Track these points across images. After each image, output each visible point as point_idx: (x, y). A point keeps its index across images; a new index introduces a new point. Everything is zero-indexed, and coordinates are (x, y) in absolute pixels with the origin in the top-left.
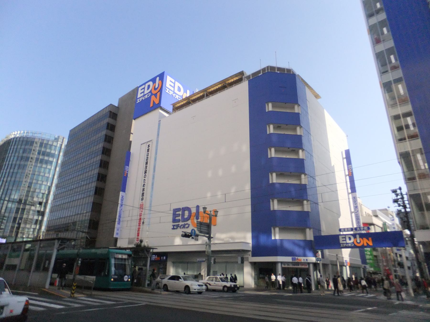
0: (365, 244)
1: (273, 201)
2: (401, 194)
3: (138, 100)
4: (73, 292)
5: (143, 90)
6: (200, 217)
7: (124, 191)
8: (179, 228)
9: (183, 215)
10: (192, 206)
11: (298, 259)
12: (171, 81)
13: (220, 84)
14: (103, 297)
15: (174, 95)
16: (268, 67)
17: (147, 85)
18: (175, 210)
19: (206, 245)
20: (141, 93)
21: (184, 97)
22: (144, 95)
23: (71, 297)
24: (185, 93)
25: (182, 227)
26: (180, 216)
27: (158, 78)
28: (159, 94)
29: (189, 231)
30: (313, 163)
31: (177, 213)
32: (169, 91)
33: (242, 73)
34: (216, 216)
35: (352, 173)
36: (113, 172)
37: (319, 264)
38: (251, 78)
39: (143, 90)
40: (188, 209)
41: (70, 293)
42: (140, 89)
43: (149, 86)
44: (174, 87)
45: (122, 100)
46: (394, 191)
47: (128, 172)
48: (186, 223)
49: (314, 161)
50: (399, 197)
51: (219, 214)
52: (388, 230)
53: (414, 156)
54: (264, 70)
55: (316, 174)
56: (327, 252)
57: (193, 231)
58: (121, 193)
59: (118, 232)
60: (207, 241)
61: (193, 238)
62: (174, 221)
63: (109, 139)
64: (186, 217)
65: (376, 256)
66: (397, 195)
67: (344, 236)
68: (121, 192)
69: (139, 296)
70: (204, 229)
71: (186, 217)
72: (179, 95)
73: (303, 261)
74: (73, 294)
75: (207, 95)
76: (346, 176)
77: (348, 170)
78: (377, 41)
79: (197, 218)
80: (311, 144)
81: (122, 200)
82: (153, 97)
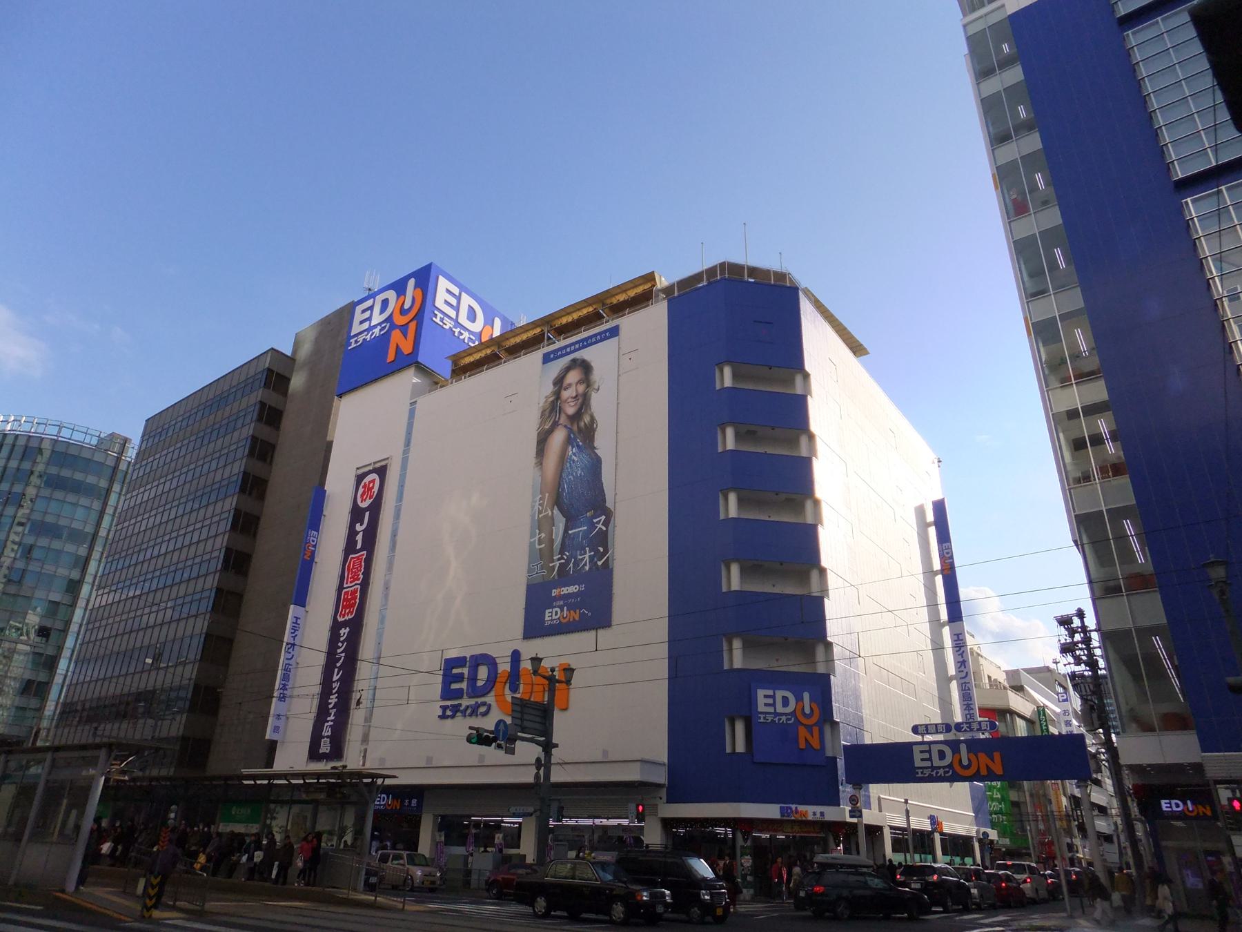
0: (984, 772)
2: (1084, 629)
3: (353, 341)
4: (149, 903)
9: (473, 678)
11: (797, 811)
12: (448, 291)
14: (234, 920)
15: (457, 331)
16: (722, 265)
18: (450, 664)
19: (538, 769)
20: (361, 322)
22: (371, 328)
24: (489, 327)
25: (469, 711)
26: (461, 680)
27: (412, 282)
28: (413, 326)
29: (488, 724)
32: (442, 320)
33: (650, 278)
34: (568, 682)
36: (269, 546)
39: (367, 314)
42: (359, 309)
43: (385, 303)
44: (457, 309)
46: (1064, 622)
47: (315, 546)
48: (480, 700)
50: (1078, 637)
52: (1054, 730)
54: (711, 271)
57: (502, 727)
59: (278, 723)
61: (499, 746)
62: (447, 693)
63: (262, 450)
64: (480, 683)
66: (1072, 632)
67: (926, 747)
68: (292, 606)
71: (480, 683)
73: (810, 817)
82: (396, 335)
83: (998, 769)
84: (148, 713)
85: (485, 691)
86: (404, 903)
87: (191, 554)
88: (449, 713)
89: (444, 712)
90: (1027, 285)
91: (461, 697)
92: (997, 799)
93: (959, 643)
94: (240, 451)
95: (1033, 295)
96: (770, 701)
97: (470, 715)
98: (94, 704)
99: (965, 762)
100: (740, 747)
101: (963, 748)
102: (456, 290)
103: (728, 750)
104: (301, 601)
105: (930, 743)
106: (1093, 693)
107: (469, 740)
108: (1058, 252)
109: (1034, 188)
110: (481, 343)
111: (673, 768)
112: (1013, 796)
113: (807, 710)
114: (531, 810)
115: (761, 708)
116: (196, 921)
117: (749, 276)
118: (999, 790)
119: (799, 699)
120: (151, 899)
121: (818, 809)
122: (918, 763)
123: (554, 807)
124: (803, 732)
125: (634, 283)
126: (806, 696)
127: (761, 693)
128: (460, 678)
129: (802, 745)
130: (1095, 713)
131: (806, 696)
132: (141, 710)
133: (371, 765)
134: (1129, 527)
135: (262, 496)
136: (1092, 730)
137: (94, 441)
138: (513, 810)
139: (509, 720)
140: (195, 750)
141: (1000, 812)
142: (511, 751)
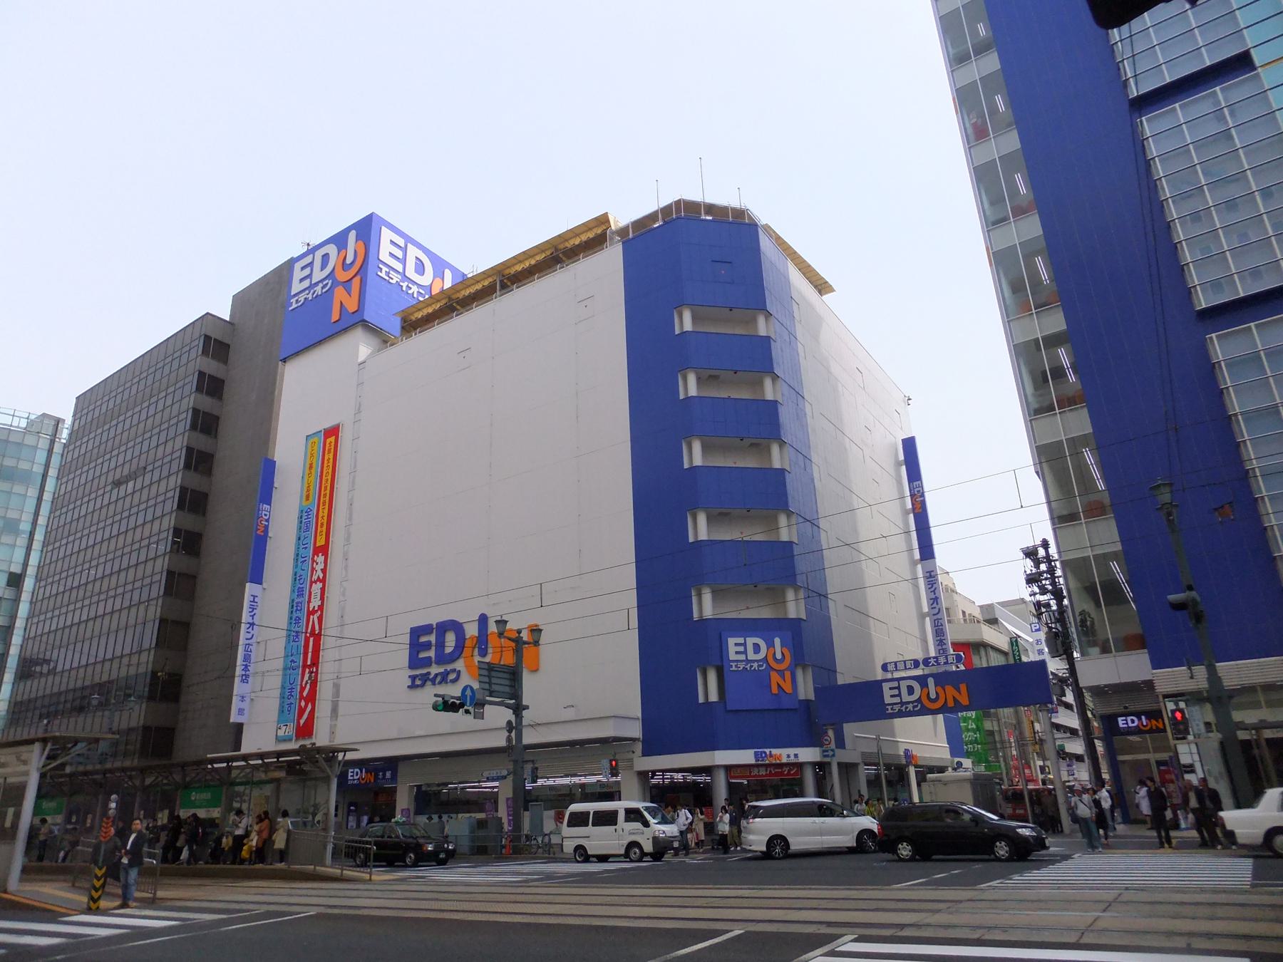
0: (951, 704)
1: (699, 595)
2: (1048, 559)
3: (293, 300)
4: (96, 895)
5: (307, 271)
6: (490, 650)
7: (258, 579)
8: (429, 683)
9: (441, 644)
10: (468, 618)
11: (771, 755)
12: (392, 242)
13: (543, 251)
14: (178, 904)
15: (404, 285)
16: (678, 203)
17: (319, 254)
18: (416, 632)
19: (510, 731)
20: (301, 280)
21: (436, 291)
22: (312, 286)
23: (89, 911)
24: (438, 280)
25: (439, 679)
26: (430, 649)
27: (353, 235)
28: (357, 281)
29: (454, 691)
30: (813, 480)
31: (423, 639)
32: (388, 274)
33: (603, 220)
34: (536, 643)
35: (923, 503)
36: (222, 524)
37: (829, 764)
38: (631, 236)
39: (307, 271)
40: (456, 627)
41: (85, 899)
42: (298, 266)
43: (326, 257)
44: (403, 261)
45: (240, 300)
46: (1030, 553)
47: (267, 520)
48: (449, 667)
49: (816, 475)
50: (1043, 567)
51: (544, 639)
52: (1024, 659)
53: (1077, 455)
54: (666, 210)
55: (821, 513)
56: (853, 730)
57: (468, 692)
58: (250, 588)
59: (242, 705)
60: (513, 718)
61: (467, 712)
62: (414, 662)
63: (205, 423)
64: (448, 650)
65: (991, 733)
66: (1037, 563)
67: (895, 684)
68: (248, 585)
69: (366, 893)
70: (501, 683)
71: (448, 650)
72: (419, 286)
73: (784, 760)
74: (95, 901)
75: (504, 287)
76: (906, 513)
77: (912, 496)
78: (976, 134)
79: (483, 653)
80: (804, 427)
81: (253, 609)
82: (340, 293)
83: (964, 700)
84: (103, 705)
85: (453, 658)
86: (371, 874)
87: (138, 537)
88: (418, 682)
89: (413, 681)
90: (988, 213)
91: (430, 665)
92: (972, 730)
93: (931, 578)
94: (181, 425)
95: (994, 223)
96: (741, 649)
97: (440, 683)
98: (46, 702)
99: (933, 696)
100: (714, 697)
101: (931, 681)
102: (401, 242)
103: (701, 700)
104: (257, 578)
105: (899, 680)
106: (1058, 621)
107: (435, 708)
108: (1018, 178)
109: (993, 110)
110: (431, 297)
111: (648, 721)
112: (988, 725)
113: (779, 656)
114: (505, 773)
115: (732, 656)
116: (145, 908)
117: (707, 213)
118: (973, 720)
119: (770, 645)
120: (97, 890)
121: (792, 751)
122: (888, 700)
123: (528, 768)
124: (775, 678)
125: (586, 226)
126: (777, 641)
127: (732, 641)
128: (427, 646)
129: (775, 690)
130: (1060, 643)
131: (777, 641)
132: (95, 702)
133: (339, 741)
134: (1089, 457)
135: (208, 472)
136: (1054, 653)
137: (23, 424)
138: (486, 774)
139: (476, 686)
140: (158, 740)
141: (976, 742)
142: (480, 716)
